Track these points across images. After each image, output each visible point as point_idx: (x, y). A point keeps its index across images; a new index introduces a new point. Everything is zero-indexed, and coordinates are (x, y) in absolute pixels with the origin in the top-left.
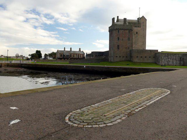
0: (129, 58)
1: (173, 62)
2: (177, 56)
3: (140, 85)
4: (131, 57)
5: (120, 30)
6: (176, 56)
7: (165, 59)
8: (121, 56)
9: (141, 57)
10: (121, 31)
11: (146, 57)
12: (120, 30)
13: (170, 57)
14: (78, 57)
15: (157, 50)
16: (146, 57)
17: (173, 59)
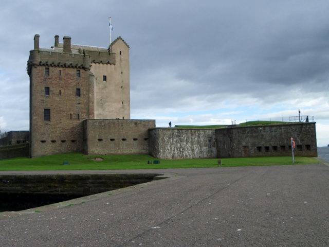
0: (79, 141)
1: (193, 150)
2: (202, 133)
3: (175, 140)
4: (84, 140)
5: (50, 68)
6: (199, 134)
7: (173, 144)
8: (54, 139)
9: (112, 140)
10: (54, 71)
11: (124, 140)
12: (50, 68)
13: (184, 137)
14: (193, 153)
15: (154, 121)
16: (124, 140)
17: (192, 143)
